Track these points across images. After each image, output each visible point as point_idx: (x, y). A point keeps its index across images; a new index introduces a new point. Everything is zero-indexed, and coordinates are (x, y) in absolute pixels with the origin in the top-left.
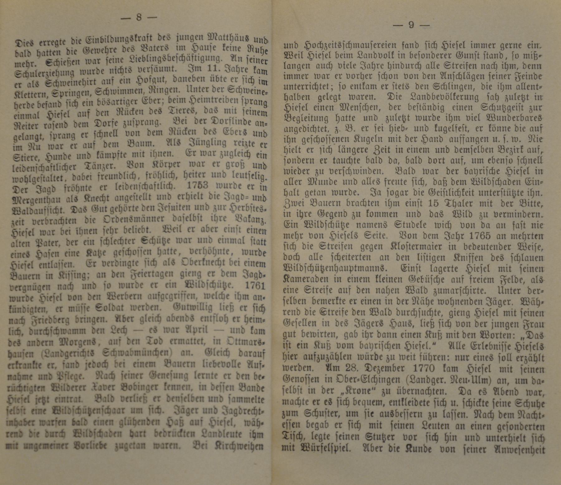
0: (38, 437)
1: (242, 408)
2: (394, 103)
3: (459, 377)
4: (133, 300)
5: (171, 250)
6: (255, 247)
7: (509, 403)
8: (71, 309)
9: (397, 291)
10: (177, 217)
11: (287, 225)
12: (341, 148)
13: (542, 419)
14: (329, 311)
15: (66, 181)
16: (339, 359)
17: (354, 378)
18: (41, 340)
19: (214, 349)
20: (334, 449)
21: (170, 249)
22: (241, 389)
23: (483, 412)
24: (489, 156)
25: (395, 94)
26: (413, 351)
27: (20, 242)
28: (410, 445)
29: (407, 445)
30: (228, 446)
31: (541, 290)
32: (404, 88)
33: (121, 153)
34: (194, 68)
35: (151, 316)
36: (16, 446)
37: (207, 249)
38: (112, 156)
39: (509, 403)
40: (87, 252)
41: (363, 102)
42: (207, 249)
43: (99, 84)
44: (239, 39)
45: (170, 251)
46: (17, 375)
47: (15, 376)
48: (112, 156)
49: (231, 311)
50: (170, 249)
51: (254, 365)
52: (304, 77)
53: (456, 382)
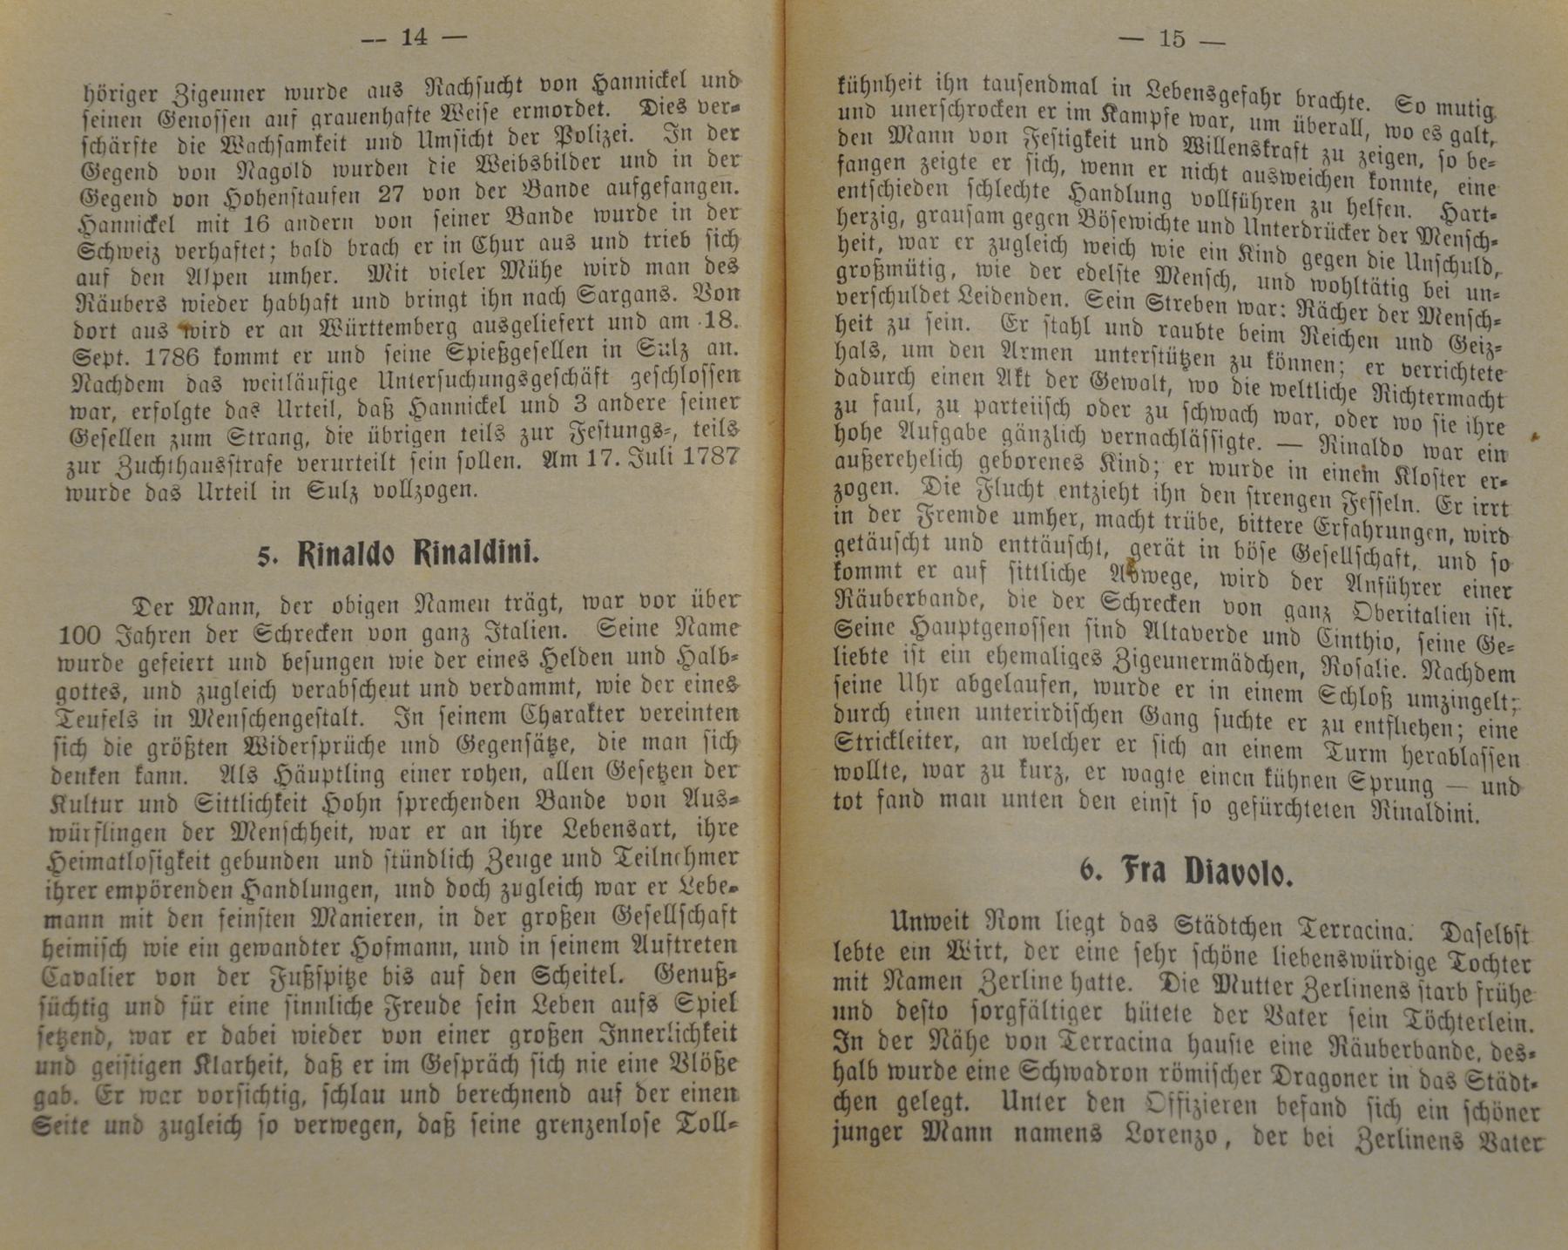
1: (1108, 1067)
3: (1008, 914)
6: (1222, 1031)
7: (1461, 643)
9: (578, 1036)
13: (1533, 1092)
14: (859, 739)
15: (880, 250)
16: (349, 1103)
20: (461, 1067)
24: (1164, 1059)
26: (342, 817)
28: (206, 1055)
29: (198, 1058)
30: (1282, 809)
34: (850, 1042)
35: (215, 1118)
37: (96, 89)
38: (135, 893)
39: (1461, 643)
41: (1223, 1060)
42: (96, 89)
44: (1363, 1052)
46: (59, 1090)
47: (55, 1093)
48: (135, 893)
51: (916, 433)
52: (478, 1038)
53: (945, 1048)
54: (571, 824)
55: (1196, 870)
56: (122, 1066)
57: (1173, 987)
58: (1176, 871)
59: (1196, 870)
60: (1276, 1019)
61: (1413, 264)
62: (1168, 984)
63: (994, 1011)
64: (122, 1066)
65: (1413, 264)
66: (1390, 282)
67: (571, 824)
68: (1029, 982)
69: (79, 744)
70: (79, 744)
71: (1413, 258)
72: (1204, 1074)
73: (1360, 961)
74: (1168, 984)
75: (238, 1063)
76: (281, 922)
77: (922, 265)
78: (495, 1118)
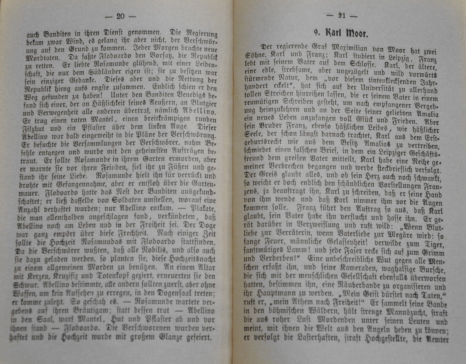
0: (55, 339)
2: (175, 37)
4: (318, 296)
5: (254, 284)
8: (342, 217)
10: (115, 240)
11: (246, 319)
12: (302, 132)
17: (210, 328)
18: (355, 283)
19: (167, 334)
21: (253, 283)
22: (428, 306)
23: (395, 310)
25: (111, 78)
27: (401, 338)
31: (213, 327)
32: (195, 260)
33: (329, 336)
36: (41, 337)
40: (29, 276)
43: (126, 321)
45: (253, 285)
49: (143, 340)
50: (253, 283)
54: (281, 116)
55: (350, 32)
56: (323, 225)
57: (110, 329)
58: (344, 33)
59: (350, 32)
60: (263, 259)
61: (363, 88)
62: (108, 328)
63: (153, 328)
64: (323, 225)
65: (363, 88)
66: (270, 248)
67: (281, 116)
68: (358, 235)
69: (264, 275)
70: (264, 275)
71: (363, 86)
72: (286, 311)
73: (115, 56)
74: (108, 328)
75: (186, 301)
76: (160, 159)
77: (269, 249)
78: (358, 174)
